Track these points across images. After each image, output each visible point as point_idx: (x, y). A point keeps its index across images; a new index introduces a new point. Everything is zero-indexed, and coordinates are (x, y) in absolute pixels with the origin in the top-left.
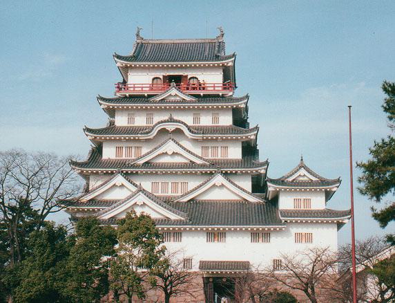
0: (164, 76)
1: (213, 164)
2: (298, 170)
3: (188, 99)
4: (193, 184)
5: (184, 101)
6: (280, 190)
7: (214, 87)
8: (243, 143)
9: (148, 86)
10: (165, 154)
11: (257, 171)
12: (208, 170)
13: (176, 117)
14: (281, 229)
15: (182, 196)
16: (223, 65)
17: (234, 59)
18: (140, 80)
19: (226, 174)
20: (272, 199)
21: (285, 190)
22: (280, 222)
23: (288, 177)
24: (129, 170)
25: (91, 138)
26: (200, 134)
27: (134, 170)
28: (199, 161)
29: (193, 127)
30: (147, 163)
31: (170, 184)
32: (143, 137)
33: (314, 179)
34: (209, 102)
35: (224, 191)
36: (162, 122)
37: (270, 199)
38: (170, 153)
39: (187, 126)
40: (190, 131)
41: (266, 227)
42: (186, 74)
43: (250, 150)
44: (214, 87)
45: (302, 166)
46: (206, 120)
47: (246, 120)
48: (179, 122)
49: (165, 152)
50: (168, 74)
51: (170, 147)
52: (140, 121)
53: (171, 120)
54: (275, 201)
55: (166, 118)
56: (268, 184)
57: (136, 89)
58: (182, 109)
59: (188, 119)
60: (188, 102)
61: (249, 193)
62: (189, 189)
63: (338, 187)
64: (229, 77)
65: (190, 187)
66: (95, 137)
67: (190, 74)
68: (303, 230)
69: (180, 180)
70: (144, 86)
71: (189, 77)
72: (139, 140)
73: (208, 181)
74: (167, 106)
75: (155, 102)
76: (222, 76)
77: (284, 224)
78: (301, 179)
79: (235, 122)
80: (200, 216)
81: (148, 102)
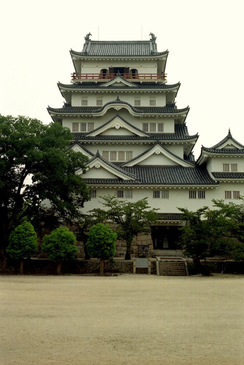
1: (153, 136)
4: (136, 152)
5: (127, 87)
6: (213, 157)
7: (151, 77)
9: (98, 75)
10: (114, 128)
12: (149, 141)
13: (122, 99)
15: (127, 163)
17: (167, 54)
18: (92, 71)
19: (163, 145)
20: (202, 164)
22: (213, 183)
24: (85, 141)
25: (52, 115)
26: (142, 112)
27: (89, 141)
28: (141, 135)
30: (99, 135)
31: (117, 153)
32: (95, 115)
34: (83, 88)
36: (110, 103)
38: (117, 127)
40: (133, 110)
41: (203, 186)
42: (128, 67)
44: (87, 77)
45: (229, 137)
46: (145, 103)
47: (174, 104)
48: (125, 103)
49: (113, 127)
50: (113, 66)
51: (118, 123)
52: (92, 103)
53: (118, 101)
57: (88, 78)
58: (106, 93)
59: (131, 101)
61: (182, 160)
62: (133, 157)
65: (135, 156)
66: (57, 115)
67: (131, 67)
71: (130, 69)
72: (92, 118)
73: (149, 150)
74: (117, 92)
76: (156, 68)
78: (228, 147)
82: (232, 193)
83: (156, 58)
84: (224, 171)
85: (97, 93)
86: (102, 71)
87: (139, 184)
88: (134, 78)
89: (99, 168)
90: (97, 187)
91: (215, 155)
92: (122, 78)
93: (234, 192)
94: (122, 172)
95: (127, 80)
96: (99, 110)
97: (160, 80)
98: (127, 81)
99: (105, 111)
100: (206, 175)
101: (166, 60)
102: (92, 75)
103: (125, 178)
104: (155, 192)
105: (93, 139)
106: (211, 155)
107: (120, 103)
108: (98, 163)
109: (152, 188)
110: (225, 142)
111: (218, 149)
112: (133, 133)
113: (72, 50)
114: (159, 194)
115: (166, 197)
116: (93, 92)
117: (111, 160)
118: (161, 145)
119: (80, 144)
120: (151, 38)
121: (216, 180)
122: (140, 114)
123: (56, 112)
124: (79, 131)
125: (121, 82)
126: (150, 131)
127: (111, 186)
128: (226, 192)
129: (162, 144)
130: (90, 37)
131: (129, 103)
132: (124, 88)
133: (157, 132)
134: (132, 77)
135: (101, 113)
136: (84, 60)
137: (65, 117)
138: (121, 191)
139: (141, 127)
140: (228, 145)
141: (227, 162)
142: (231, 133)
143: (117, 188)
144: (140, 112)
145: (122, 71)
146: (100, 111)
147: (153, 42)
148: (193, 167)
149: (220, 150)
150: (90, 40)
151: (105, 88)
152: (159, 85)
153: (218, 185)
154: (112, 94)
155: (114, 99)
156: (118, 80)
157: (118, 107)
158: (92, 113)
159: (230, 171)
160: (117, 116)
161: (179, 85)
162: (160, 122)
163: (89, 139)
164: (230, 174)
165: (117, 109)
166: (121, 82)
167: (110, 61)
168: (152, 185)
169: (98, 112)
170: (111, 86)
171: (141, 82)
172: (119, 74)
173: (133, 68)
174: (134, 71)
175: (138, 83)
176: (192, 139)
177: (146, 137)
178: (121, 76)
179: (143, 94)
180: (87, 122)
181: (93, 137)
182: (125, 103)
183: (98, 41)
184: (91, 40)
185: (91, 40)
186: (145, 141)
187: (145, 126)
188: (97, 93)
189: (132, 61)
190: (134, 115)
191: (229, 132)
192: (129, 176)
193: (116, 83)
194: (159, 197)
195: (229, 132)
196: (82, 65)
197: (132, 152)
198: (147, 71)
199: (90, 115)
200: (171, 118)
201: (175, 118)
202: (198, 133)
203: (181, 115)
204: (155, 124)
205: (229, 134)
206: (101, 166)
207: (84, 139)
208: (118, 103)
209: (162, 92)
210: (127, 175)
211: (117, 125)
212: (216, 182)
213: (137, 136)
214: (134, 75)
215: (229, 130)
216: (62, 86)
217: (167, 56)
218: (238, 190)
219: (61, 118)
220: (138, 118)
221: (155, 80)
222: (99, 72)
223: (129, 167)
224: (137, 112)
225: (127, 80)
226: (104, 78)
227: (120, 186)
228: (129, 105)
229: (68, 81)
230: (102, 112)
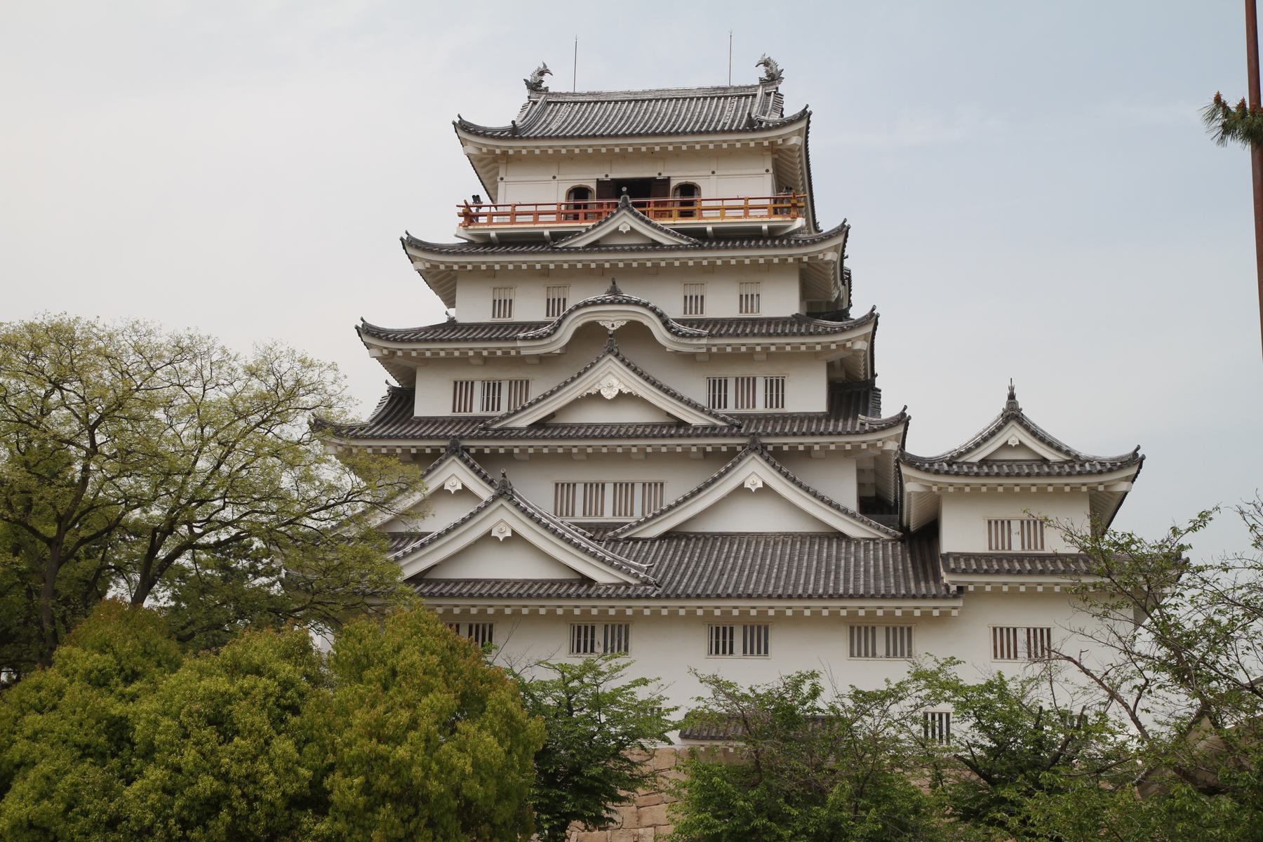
0: (599, 182)
1: (736, 425)
2: (999, 428)
3: (666, 240)
5: (655, 246)
8: (830, 366)
10: (596, 398)
11: (873, 445)
14: (945, 615)
16: (772, 143)
18: (537, 195)
19: (779, 458)
21: (960, 489)
23: (969, 451)
24: (488, 445)
26: (700, 336)
29: (683, 322)
30: (540, 424)
31: (609, 489)
32: (530, 349)
33: (1052, 456)
35: (758, 505)
36: (586, 305)
37: (912, 528)
38: (609, 394)
39: (660, 315)
40: (669, 329)
41: (899, 607)
42: (665, 175)
43: (853, 390)
44: (514, 214)
45: (1012, 415)
46: (722, 303)
49: (593, 392)
50: (613, 176)
51: (611, 378)
53: (616, 298)
54: (930, 530)
55: (600, 293)
56: (905, 470)
57: (519, 219)
60: (670, 249)
61: (853, 516)
63: (1133, 479)
64: (793, 183)
65: (683, 499)
67: (678, 175)
68: (1023, 618)
69: (638, 475)
70: (540, 208)
71: (674, 184)
72: (520, 361)
75: (569, 250)
77: (955, 597)
79: (835, 390)
80: (729, 596)
81: (554, 251)
82: (1022, 636)
83: (766, 139)
84: (990, 548)
85: (545, 273)
86: (572, 195)
87: (648, 597)
88: (684, 214)
89: (506, 539)
90: (917, 613)
91: (951, 485)
92: (636, 215)
93: (1028, 630)
94: (594, 555)
95: (659, 222)
96: (545, 329)
97: (777, 220)
98: (655, 226)
99: (566, 334)
100: (929, 566)
101: (806, 145)
102: (532, 209)
103: (602, 576)
104: (717, 629)
105: (519, 438)
106: (935, 484)
107: (620, 303)
108: (502, 521)
109: (843, 613)
110: (992, 434)
111: (964, 463)
112: (669, 414)
113: (461, 120)
114: (731, 637)
115: (759, 652)
116: (531, 267)
117: (584, 514)
118: (766, 454)
119: (466, 455)
120: (764, 76)
121: (954, 583)
122: (695, 342)
123: (388, 340)
124: (477, 411)
125: (633, 232)
126: (737, 407)
127: (543, 607)
128: (995, 629)
129: (769, 452)
130: (547, 81)
131: (662, 307)
132: (646, 251)
133: (760, 408)
134: (676, 209)
135: (552, 343)
136: (505, 153)
137: (425, 362)
138: (586, 628)
139: (702, 398)
140: (1006, 446)
141: (1001, 512)
142: (1017, 398)
143: (569, 613)
144: (692, 336)
145: (642, 192)
146: (549, 335)
147: (771, 89)
148: (886, 537)
149: (973, 464)
150: (546, 89)
151: (577, 251)
152: (773, 238)
153: (959, 603)
154: (600, 272)
155: (600, 293)
156: (625, 221)
157: (613, 317)
158: (519, 344)
159: (1016, 548)
160: (610, 351)
161: (1135, 461)
162: (774, 371)
163: (500, 438)
164: (1020, 558)
165: (608, 326)
166: (633, 232)
167: (595, 158)
168: (700, 603)
169: (541, 338)
170: (599, 246)
171: (709, 229)
172: (625, 200)
173: (683, 181)
174: (689, 190)
175: (700, 237)
176: (883, 429)
177: (714, 427)
178: (636, 210)
179: (711, 270)
180: (505, 376)
181: (520, 430)
182: (637, 303)
183: (574, 94)
184: (551, 90)
185: (551, 90)
186: (710, 442)
187: (717, 387)
188: (545, 273)
189: (678, 155)
190: (671, 347)
191: (1012, 397)
192: (619, 568)
193: (616, 232)
194: (731, 652)
195: (1012, 397)
196: (501, 175)
197: (662, 485)
198: (735, 192)
199: (513, 348)
200: (811, 356)
201: (831, 358)
202: (905, 408)
203: (849, 344)
204: (754, 379)
205: (1008, 404)
206: (513, 532)
207: (485, 438)
208: (612, 302)
209: (783, 261)
210: (611, 564)
211: (610, 387)
212: (953, 588)
213: (681, 424)
214: (691, 203)
215: (1012, 389)
216: (417, 247)
217: (807, 133)
218: (1045, 625)
219: (410, 364)
220: (689, 359)
221: (762, 219)
222: (563, 199)
223: (645, 541)
224: (684, 336)
225: (659, 222)
226: (576, 218)
227: (578, 607)
228: (653, 310)
229: (446, 230)
230: (554, 338)
